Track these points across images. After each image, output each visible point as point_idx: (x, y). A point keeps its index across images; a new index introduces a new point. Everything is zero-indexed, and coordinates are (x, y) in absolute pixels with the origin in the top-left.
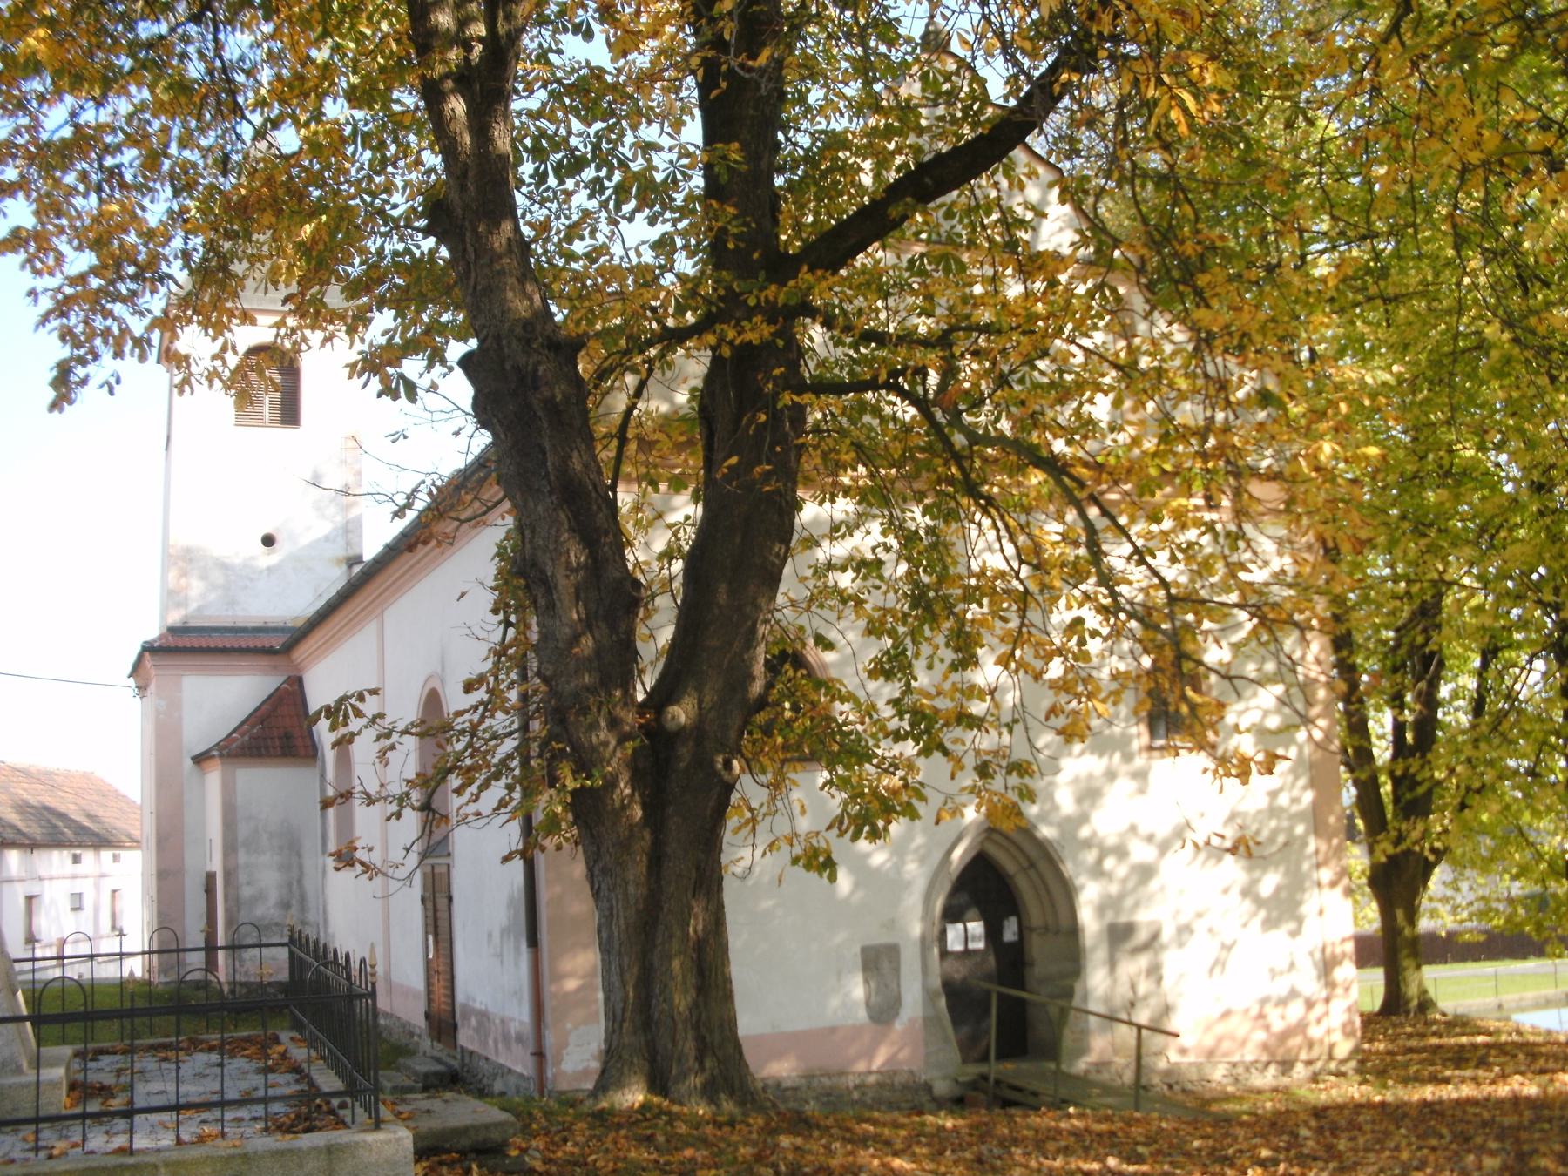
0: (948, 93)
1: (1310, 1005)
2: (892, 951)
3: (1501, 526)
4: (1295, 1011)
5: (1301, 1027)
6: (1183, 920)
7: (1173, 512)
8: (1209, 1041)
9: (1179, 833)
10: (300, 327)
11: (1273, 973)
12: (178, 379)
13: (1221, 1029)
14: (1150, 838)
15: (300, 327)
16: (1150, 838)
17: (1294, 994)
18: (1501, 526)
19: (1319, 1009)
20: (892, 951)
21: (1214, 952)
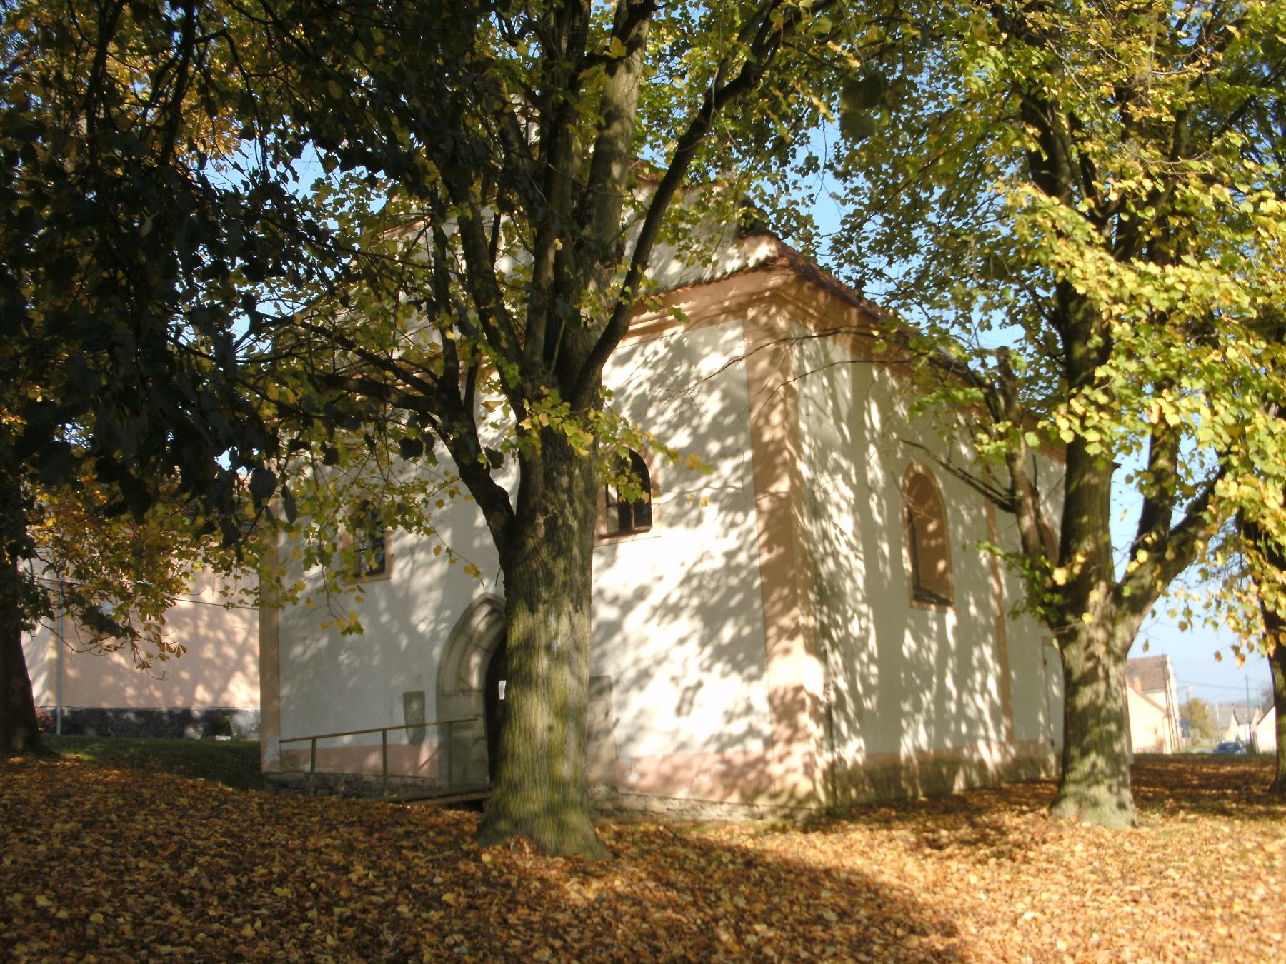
0: (997, 35)
1: (770, 742)
2: (420, 695)
3: (1258, 191)
4: (756, 747)
5: (762, 760)
6: (643, 665)
7: (1186, 327)
8: (666, 769)
9: (641, 594)
10: (1255, 406)
11: (730, 717)
12: (581, 424)
13: (678, 759)
14: (614, 601)
15: (1255, 406)
16: (614, 601)
17: (752, 732)
18: (1258, 191)
19: (780, 748)
20: (420, 695)
21: (675, 696)
